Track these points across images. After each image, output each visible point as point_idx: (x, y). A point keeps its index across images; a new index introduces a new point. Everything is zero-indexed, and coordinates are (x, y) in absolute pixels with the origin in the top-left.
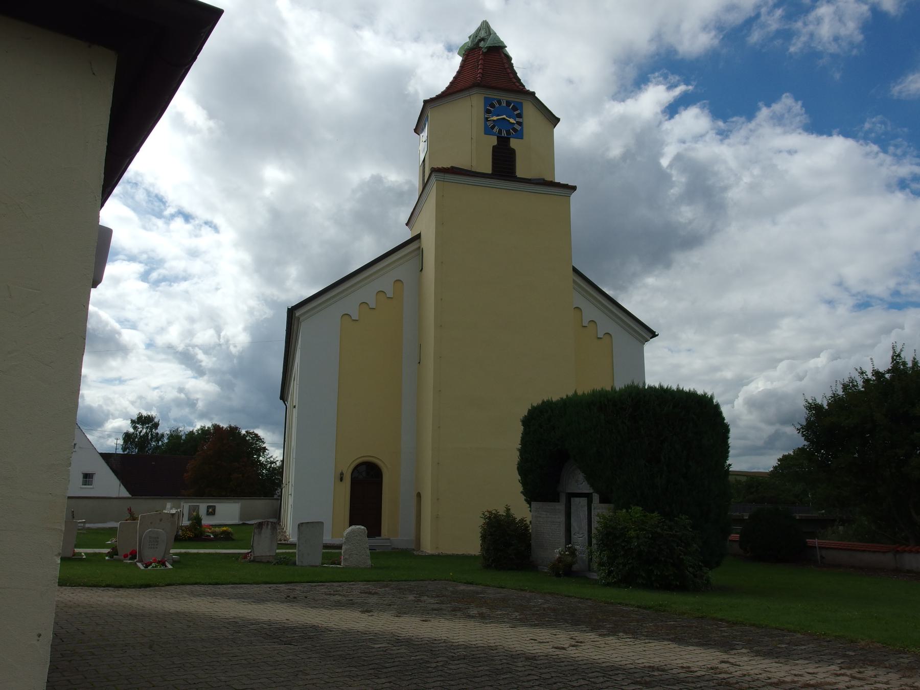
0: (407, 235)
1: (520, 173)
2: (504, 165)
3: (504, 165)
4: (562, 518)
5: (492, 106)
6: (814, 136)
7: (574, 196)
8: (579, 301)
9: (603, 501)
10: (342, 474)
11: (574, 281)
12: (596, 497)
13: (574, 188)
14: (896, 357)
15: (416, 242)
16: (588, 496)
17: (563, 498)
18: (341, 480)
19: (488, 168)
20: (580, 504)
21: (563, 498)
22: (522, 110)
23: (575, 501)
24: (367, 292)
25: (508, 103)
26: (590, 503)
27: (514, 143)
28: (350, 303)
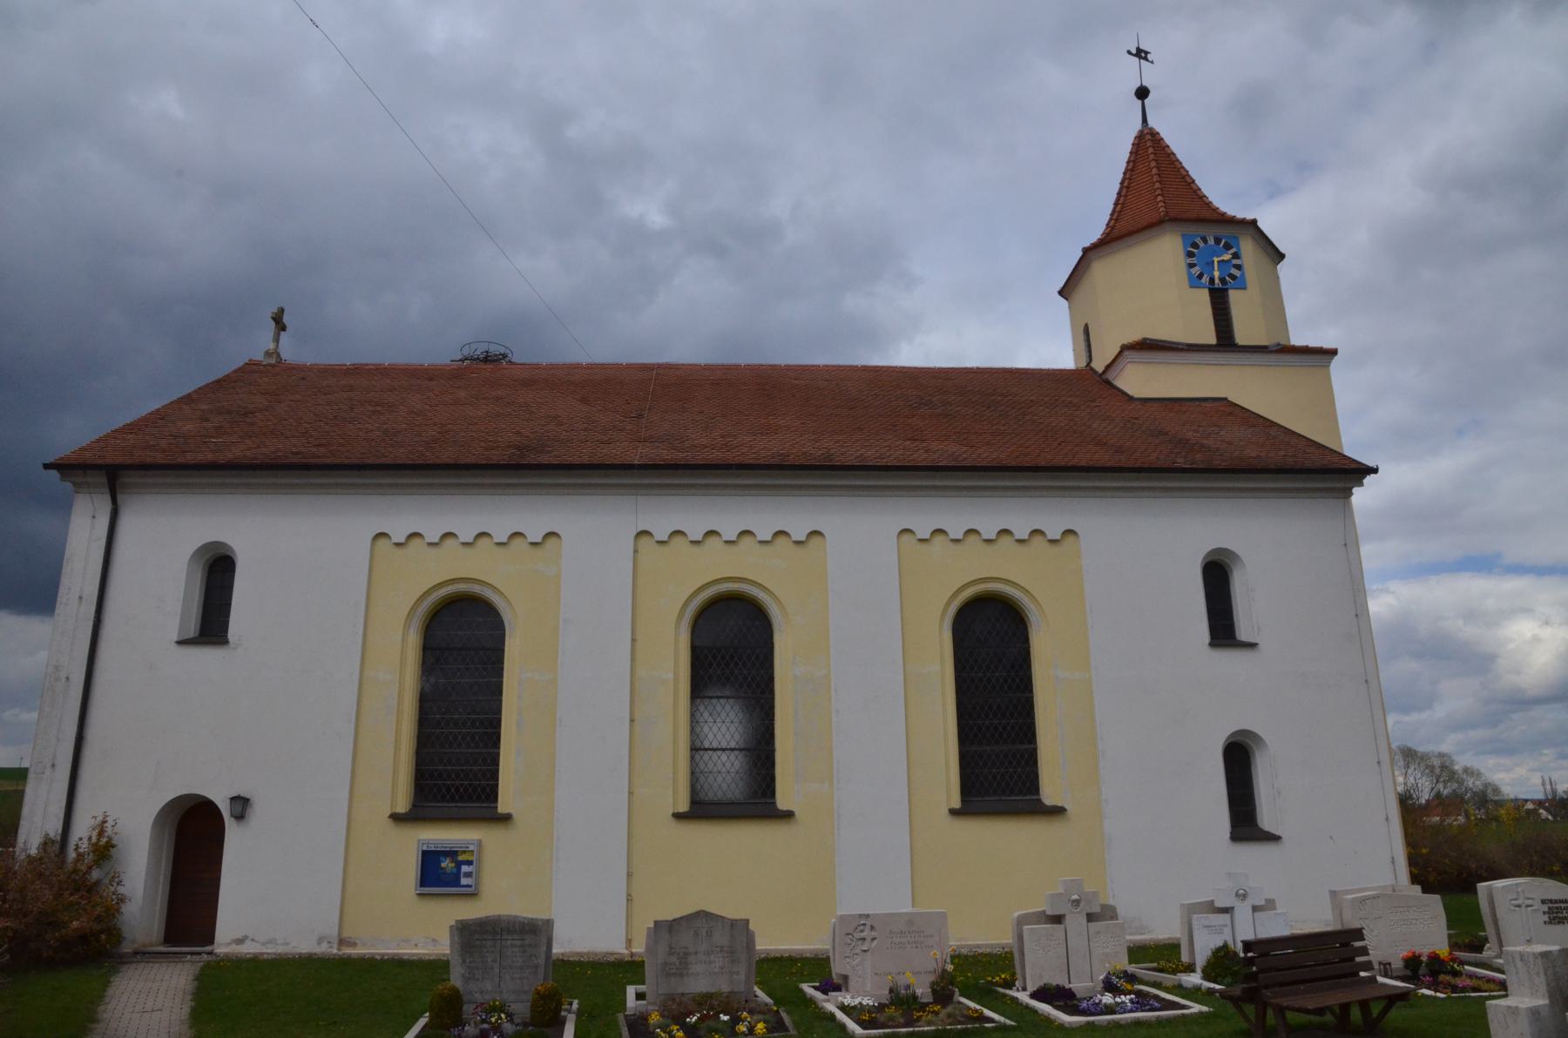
5: (1195, 245)
13: (1334, 352)
25: (1218, 241)
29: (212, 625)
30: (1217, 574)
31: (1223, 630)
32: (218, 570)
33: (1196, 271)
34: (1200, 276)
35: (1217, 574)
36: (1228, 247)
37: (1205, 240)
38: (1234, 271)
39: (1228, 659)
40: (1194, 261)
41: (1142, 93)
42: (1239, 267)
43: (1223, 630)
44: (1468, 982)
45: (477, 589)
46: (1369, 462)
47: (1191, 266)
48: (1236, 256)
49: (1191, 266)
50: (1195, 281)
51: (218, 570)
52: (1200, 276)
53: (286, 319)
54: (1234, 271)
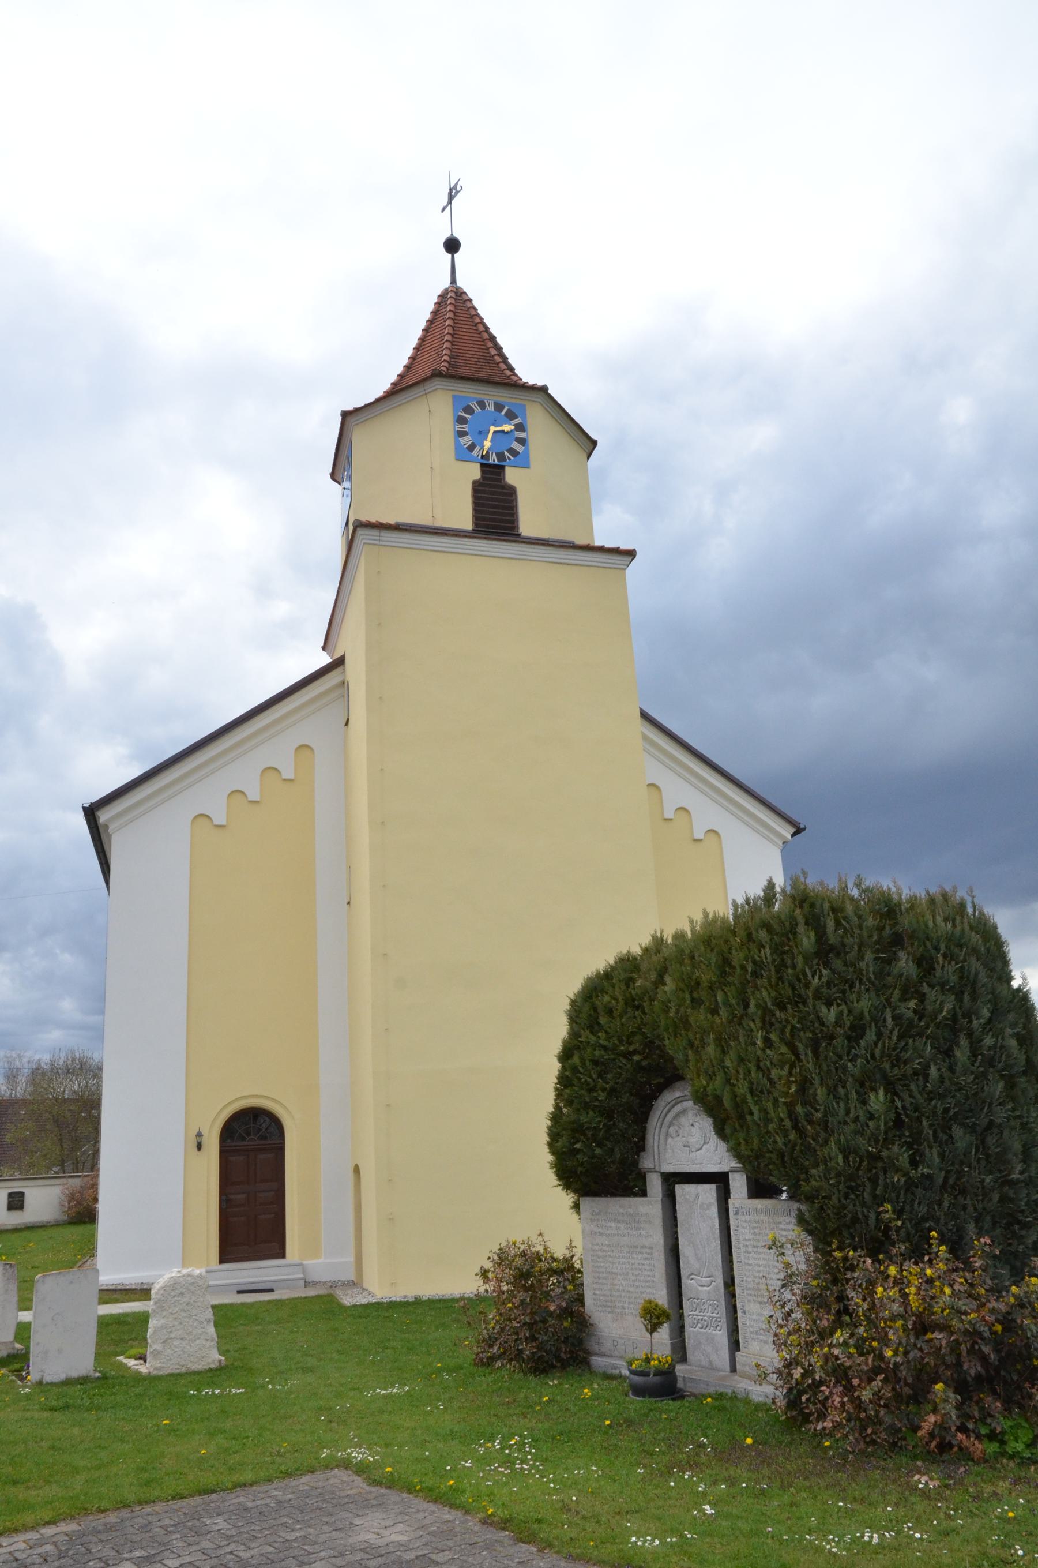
0: (325, 659)
1: (527, 526)
2: (495, 512)
3: (495, 512)
4: (657, 1238)
5: (469, 410)
6: (612, 962)
7: (634, 570)
8: (656, 772)
9: (760, 1189)
10: (199, 1135)
11: (645, 738)
12: (738, 1184)
13: (631, 554)
14: (706, 915)
15: (338, 670)
16: (720, 1180)
17: (655, 1185)
18: (199, 1147)
19: (468, 525)
20: (697, 1203)
21: (655, 1185)
22: (525, 417)
23: (682, 1191)
24: (242, 771)
25: (499, 407)
26: (724, 1195)
27: (512, 476)
28: (208, 793)
33: (466, 441)
34: (471, 448)
36: (511, 416)
37: (482, 404)
38: (516, 446)
40: (465, 428)
41: (452, 246)
42: (522, 441)
44: (346, 1500)
48: (520, 427)
49: (461, 434)
50: (464, 454)
52: (471, 448)
54: (516, 446)
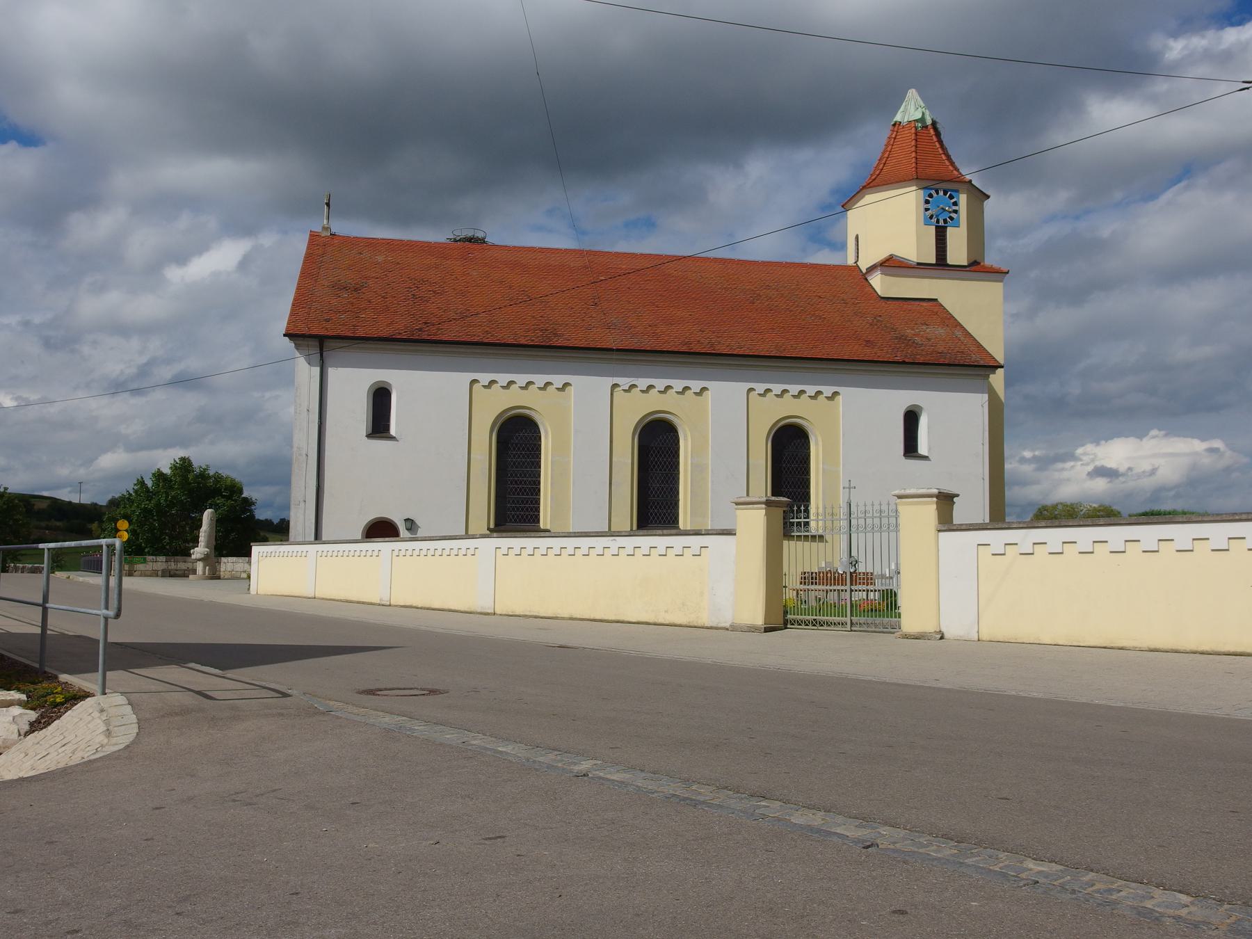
5: (930, 196)
25: (945, 193)
29: (379, 425)
30: (911, 419)
31: (910, 448)
32: (381, 398)
34: (931, 217)
35: (911, 419)
38: (953, 215)
39: (913, 463)
43: (910, 448)
45: (527, 412)
46: (956, 492)
47: (927, 210)
48: (955, 204)
49: (927, 210)
51: (381, 398)
52: (931, 217)
53: (568, 388)
